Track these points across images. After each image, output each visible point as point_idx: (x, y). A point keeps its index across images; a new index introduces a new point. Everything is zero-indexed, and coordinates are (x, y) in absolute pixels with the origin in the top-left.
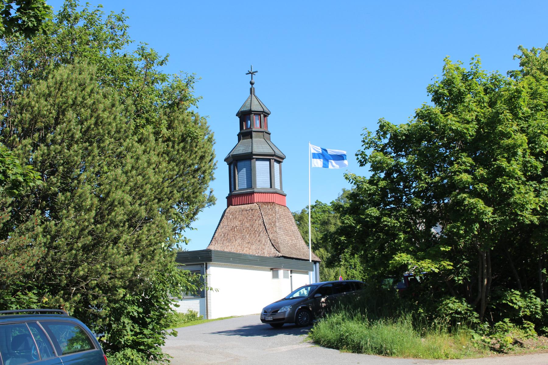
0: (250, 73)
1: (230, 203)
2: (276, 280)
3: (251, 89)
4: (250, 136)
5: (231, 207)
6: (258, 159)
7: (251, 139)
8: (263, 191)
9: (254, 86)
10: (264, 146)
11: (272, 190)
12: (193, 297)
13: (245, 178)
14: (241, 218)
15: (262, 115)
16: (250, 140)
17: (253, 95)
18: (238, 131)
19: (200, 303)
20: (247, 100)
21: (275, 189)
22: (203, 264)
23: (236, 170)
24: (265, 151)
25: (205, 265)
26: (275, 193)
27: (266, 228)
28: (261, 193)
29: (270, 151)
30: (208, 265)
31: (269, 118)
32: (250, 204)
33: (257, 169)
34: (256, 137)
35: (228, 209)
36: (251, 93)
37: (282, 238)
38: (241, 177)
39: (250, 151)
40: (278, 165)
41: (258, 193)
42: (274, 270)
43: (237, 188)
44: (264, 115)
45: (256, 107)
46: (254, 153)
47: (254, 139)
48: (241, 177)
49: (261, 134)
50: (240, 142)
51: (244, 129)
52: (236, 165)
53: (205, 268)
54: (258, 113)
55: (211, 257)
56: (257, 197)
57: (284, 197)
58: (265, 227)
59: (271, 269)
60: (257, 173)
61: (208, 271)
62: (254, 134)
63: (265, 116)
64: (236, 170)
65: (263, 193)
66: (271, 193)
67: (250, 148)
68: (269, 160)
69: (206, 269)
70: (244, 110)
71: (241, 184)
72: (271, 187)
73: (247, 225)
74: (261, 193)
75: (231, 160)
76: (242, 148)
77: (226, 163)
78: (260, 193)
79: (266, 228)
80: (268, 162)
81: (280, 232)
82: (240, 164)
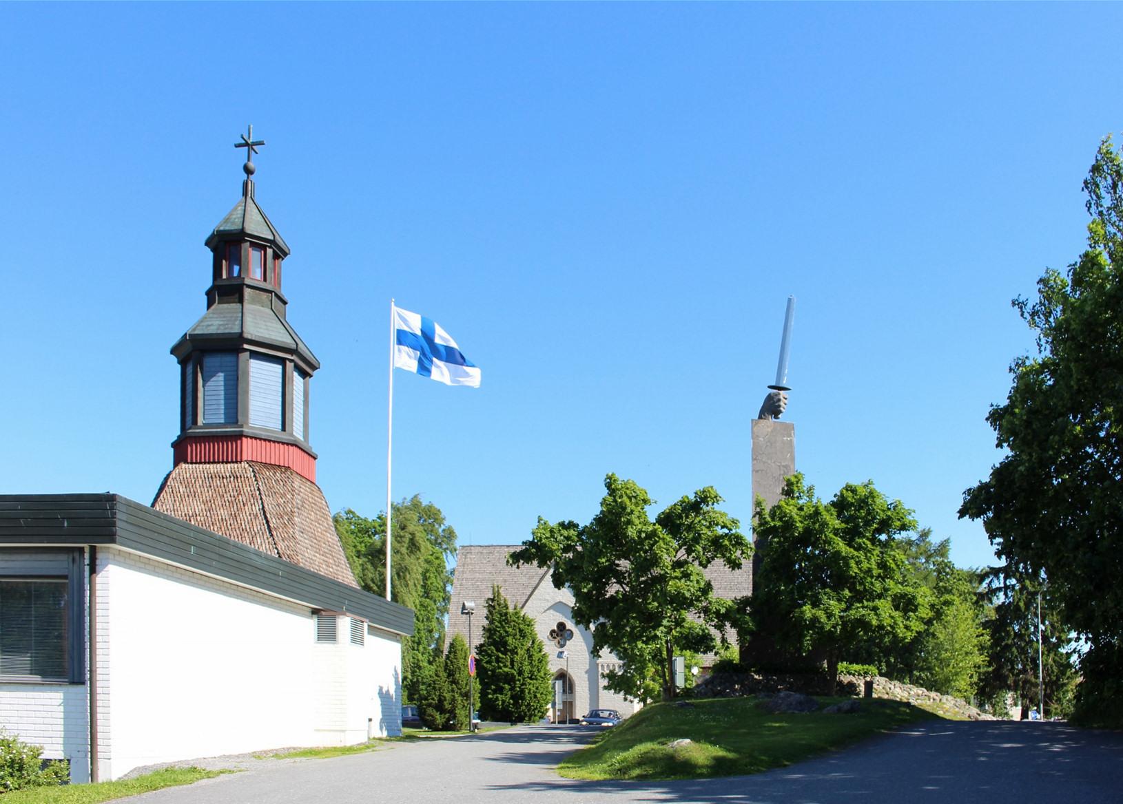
0: (247, 144)
1: (180, 456)
2: (327, 646)
3: (245, 185)
4: (237, 295)
5: (184, 465)
6: (255, 355)
7: (239, 305)
8: (264, 435)
9: (251, 177)
10: (269, 324)
11: (284, 437)
12: (38, 679)
13: (222, 397)
14: (207, 495)
15: (269, 251)
16: (237, 306)
17: (249, 200)
18: (208, 283)
19: (66, 703)
20: (235, 209)
21: (292, 435)
22: (81, 550)
23: (200, 375)
24: (273, 337)
25: (87, 556)
26: (292, 445)
27: (269, 526)
28: (260, 439)
29: (285, 340)
30: (100, 556)
31: (285, 263)
32: (232, 462)
33: (251, 379)
34: (253, 301)
35: (177, 470)
36: (245, 194)
37: (306, 555)
38: (212, 393)
39: (236, 330)
40: (302, 379)
41: (251, 438)
42: (324, 615)
43: (200, 421)
44: (274, 251)
45: (255, 226)
46: (246, 335)
47: (247, 306)
48: (212, 393)
49: (264, 296)
50: (213, 307)
51: (224, 276)
52: (199, 363)
53: (87, 569)
54: (260, 244)
55: (114, 525)
56: (249, 448)
57: (311, 459)
58: (267, 522)
59: (315, 612)
60: (251, 388)
61: (99, 579)
62: (247, 291)
63: (276, 257)
64: (200, 375)
65: (265, 440)
66: (283, 443)
67: (238, 322)
68: (282, 362)
69: (93, 571)
70: (227, 228)
71: (211, 412)
72: (284, 429)
73: (223, 513)
74: (260, 439)
75: (188, 348)
76: (217, 322)
77: (174, 359)
78: (256, 438)
79: (269, 526)
80: (278, 368)
81: (304, 541)
82: (210, 361)
